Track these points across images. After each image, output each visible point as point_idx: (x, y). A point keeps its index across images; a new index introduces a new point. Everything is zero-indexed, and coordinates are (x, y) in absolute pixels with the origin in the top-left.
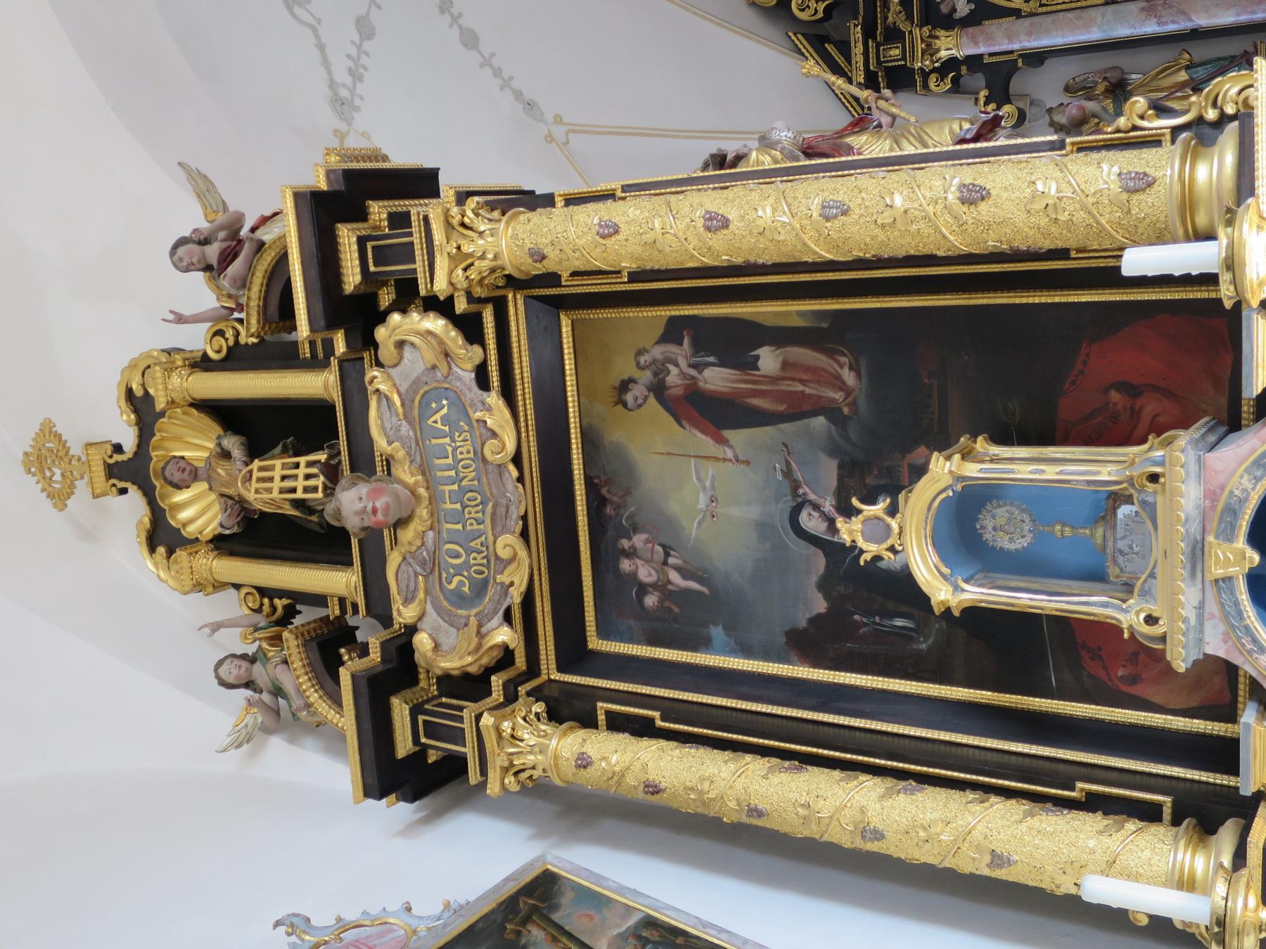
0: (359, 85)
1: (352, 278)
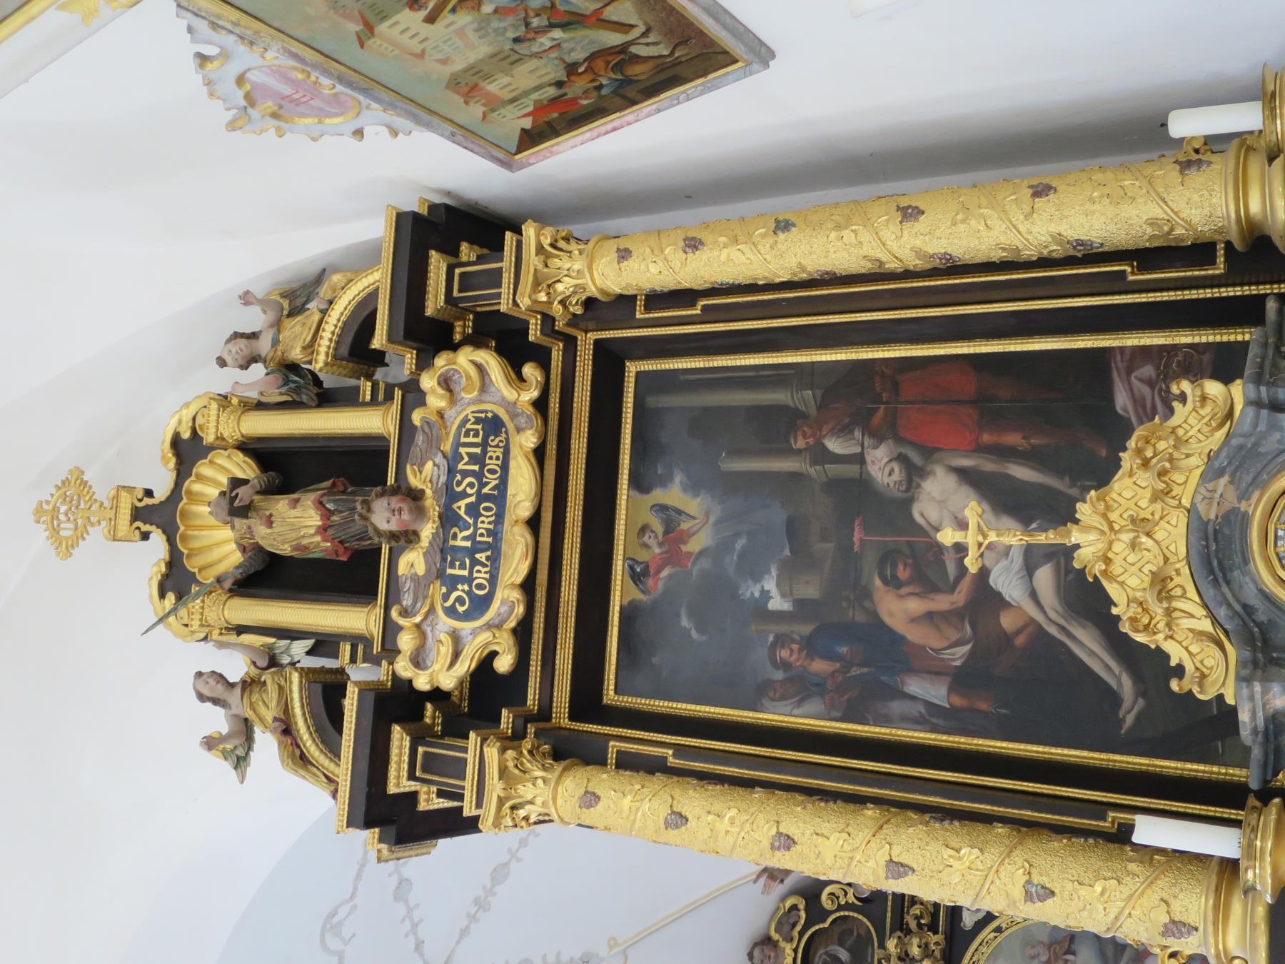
1: (434, 303)
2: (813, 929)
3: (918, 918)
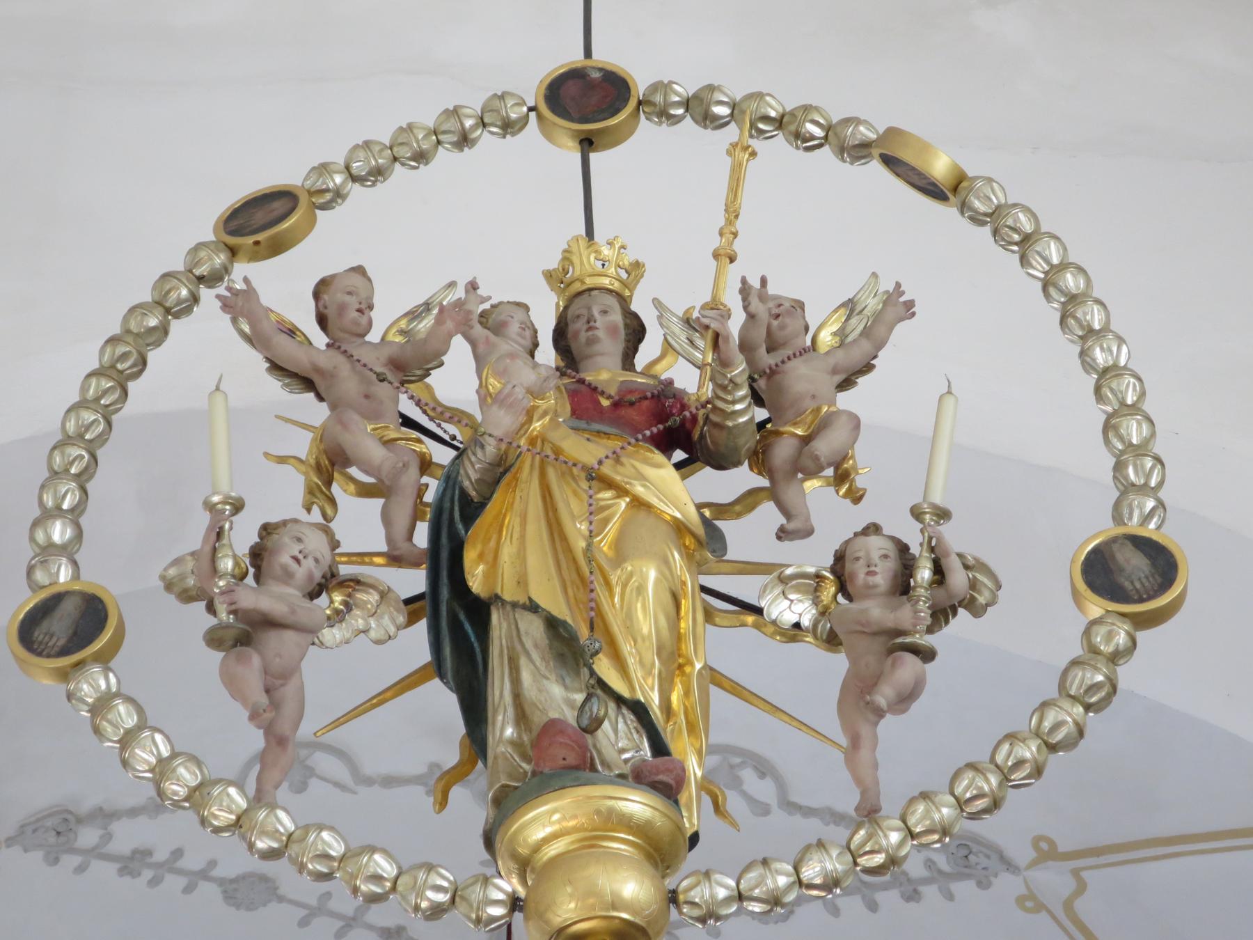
0: (113, 868)
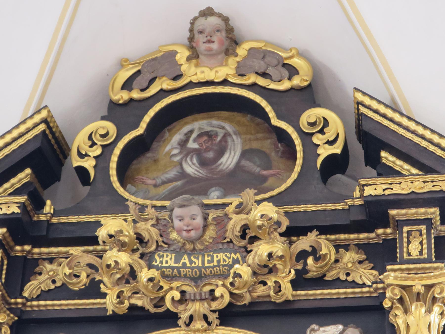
2: (264, 103)
3: (314, 252)
